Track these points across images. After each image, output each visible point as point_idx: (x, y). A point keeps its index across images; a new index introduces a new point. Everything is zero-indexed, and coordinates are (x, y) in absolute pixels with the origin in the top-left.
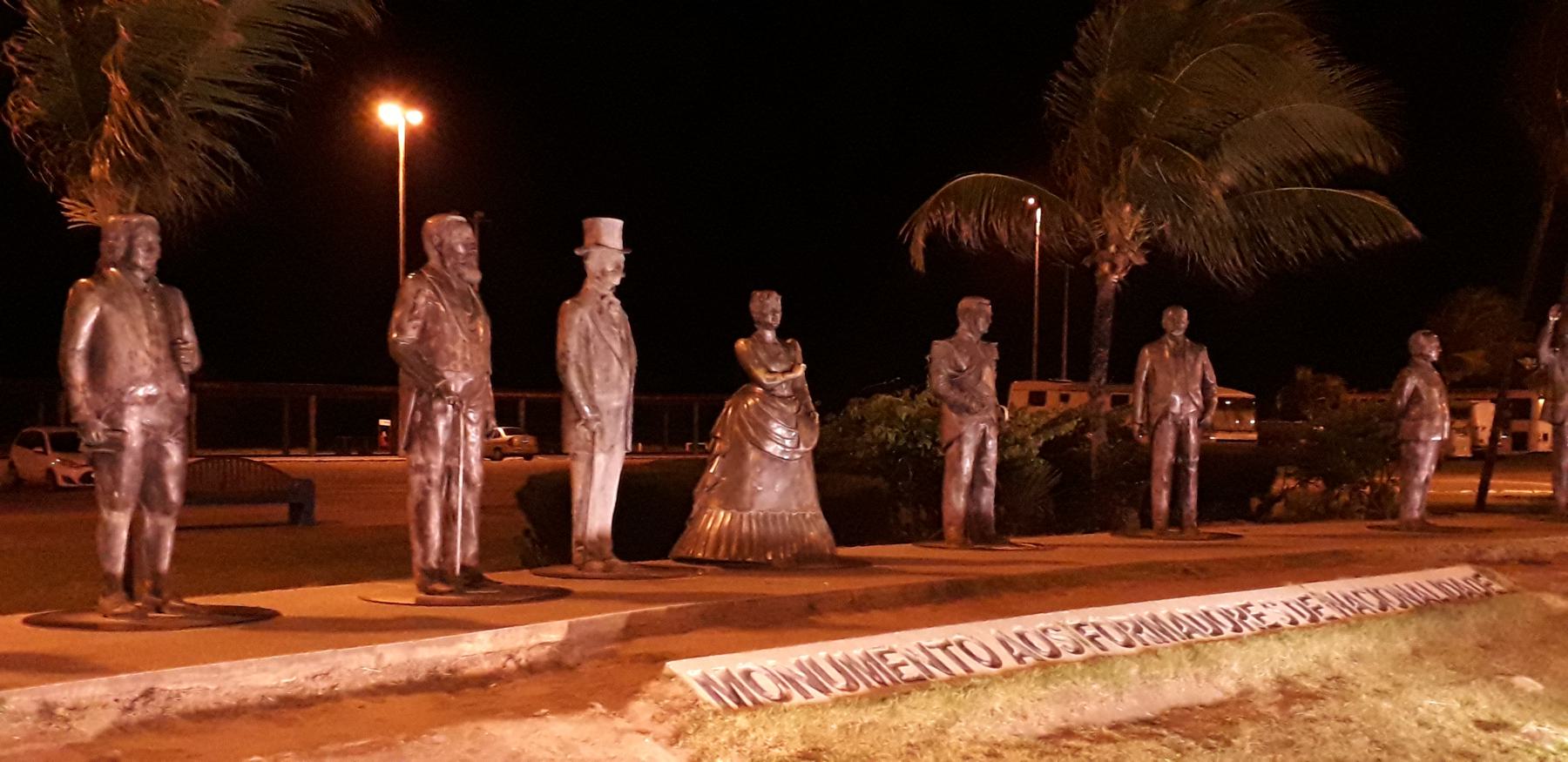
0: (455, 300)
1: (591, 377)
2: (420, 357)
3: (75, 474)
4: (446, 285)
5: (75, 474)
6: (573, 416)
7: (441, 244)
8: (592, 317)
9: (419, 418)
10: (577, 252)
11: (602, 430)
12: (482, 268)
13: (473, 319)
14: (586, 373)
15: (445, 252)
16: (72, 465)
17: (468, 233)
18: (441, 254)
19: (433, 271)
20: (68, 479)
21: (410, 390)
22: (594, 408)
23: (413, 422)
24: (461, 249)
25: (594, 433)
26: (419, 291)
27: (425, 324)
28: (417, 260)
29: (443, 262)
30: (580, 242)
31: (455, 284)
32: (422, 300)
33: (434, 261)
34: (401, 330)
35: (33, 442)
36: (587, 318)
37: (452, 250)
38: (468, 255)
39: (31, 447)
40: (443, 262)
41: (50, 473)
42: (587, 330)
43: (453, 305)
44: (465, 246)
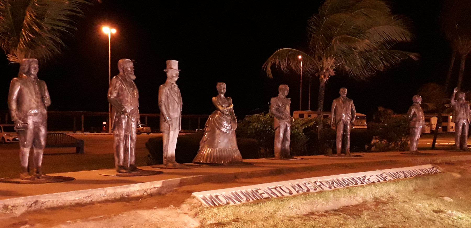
1: (169, 108)
3: (11, 138)
4: (125, 80)
7: (123, 68)
11: (172, 124)
12: (135, 74)
13: (133, 90)
15: (125, 70)
16: (10, 136)
17: (131, 64)
19: (122, 76)
20: (8, 140)
22: (170, 117)
24: (129, 69)
26: (117, 82)
27: (119, 92)
32: (118, 85)
33: (121, 73)
40: (124, 73)
41: (3, 138)
43: (127, 86)
44: (131, 68)
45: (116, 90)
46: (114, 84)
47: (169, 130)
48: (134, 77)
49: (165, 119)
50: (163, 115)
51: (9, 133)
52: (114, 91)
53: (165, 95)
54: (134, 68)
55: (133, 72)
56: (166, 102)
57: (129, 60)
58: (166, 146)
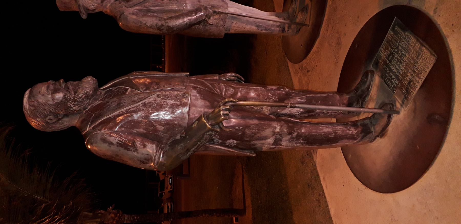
0: (114, 102)
1: (175, 11)
2: (176, 142)
3: (170, 186)
4: (99, 111)
5: (170, 186)
6: (201, 26)
7: (56, 115)
8: (131, 7)
9: (233, 142)
10: (84, 17)
11: (213, 7)
12: (79, 78)
13: (134, 87)
14: (173, 15)
15: (63, 109)
16: (167, 187)
17: (42, 88)
18: (66, 115)
19: (85, 122)
20: (171, 188)
21: (207, 148)
22: (197, 10)
23: (236, 147)
24: (59, 96)
25: (215, 12)
26: (104, 140)
27: (140, 135)
28: (75, 136)
29: (74, 113)
30: (77, 14)
31: (97, 103)
32: (114, 139)
33: (75, 121)
34: (148, 159)
35: (161, 195)
36: (131, 10)
37: (59, 104)
38: (67, 89)
39: (163, 195)
40: (74, 113)
41: (169, 192)
42: (140, 10)
43: (119, 106)
44: (56, 91)
45: (134, 145)
46: (113, 148)
47: (227, 14)
48: (89, 83)
49: (199, 23)
50: (190, 25)
51: (166, 187)
52: (136, 150)
53: (143, 16)
54: (56, 79)
55: (70, 85)
56: (159, 15)
57: (27, 92)
58: (258, 26)
